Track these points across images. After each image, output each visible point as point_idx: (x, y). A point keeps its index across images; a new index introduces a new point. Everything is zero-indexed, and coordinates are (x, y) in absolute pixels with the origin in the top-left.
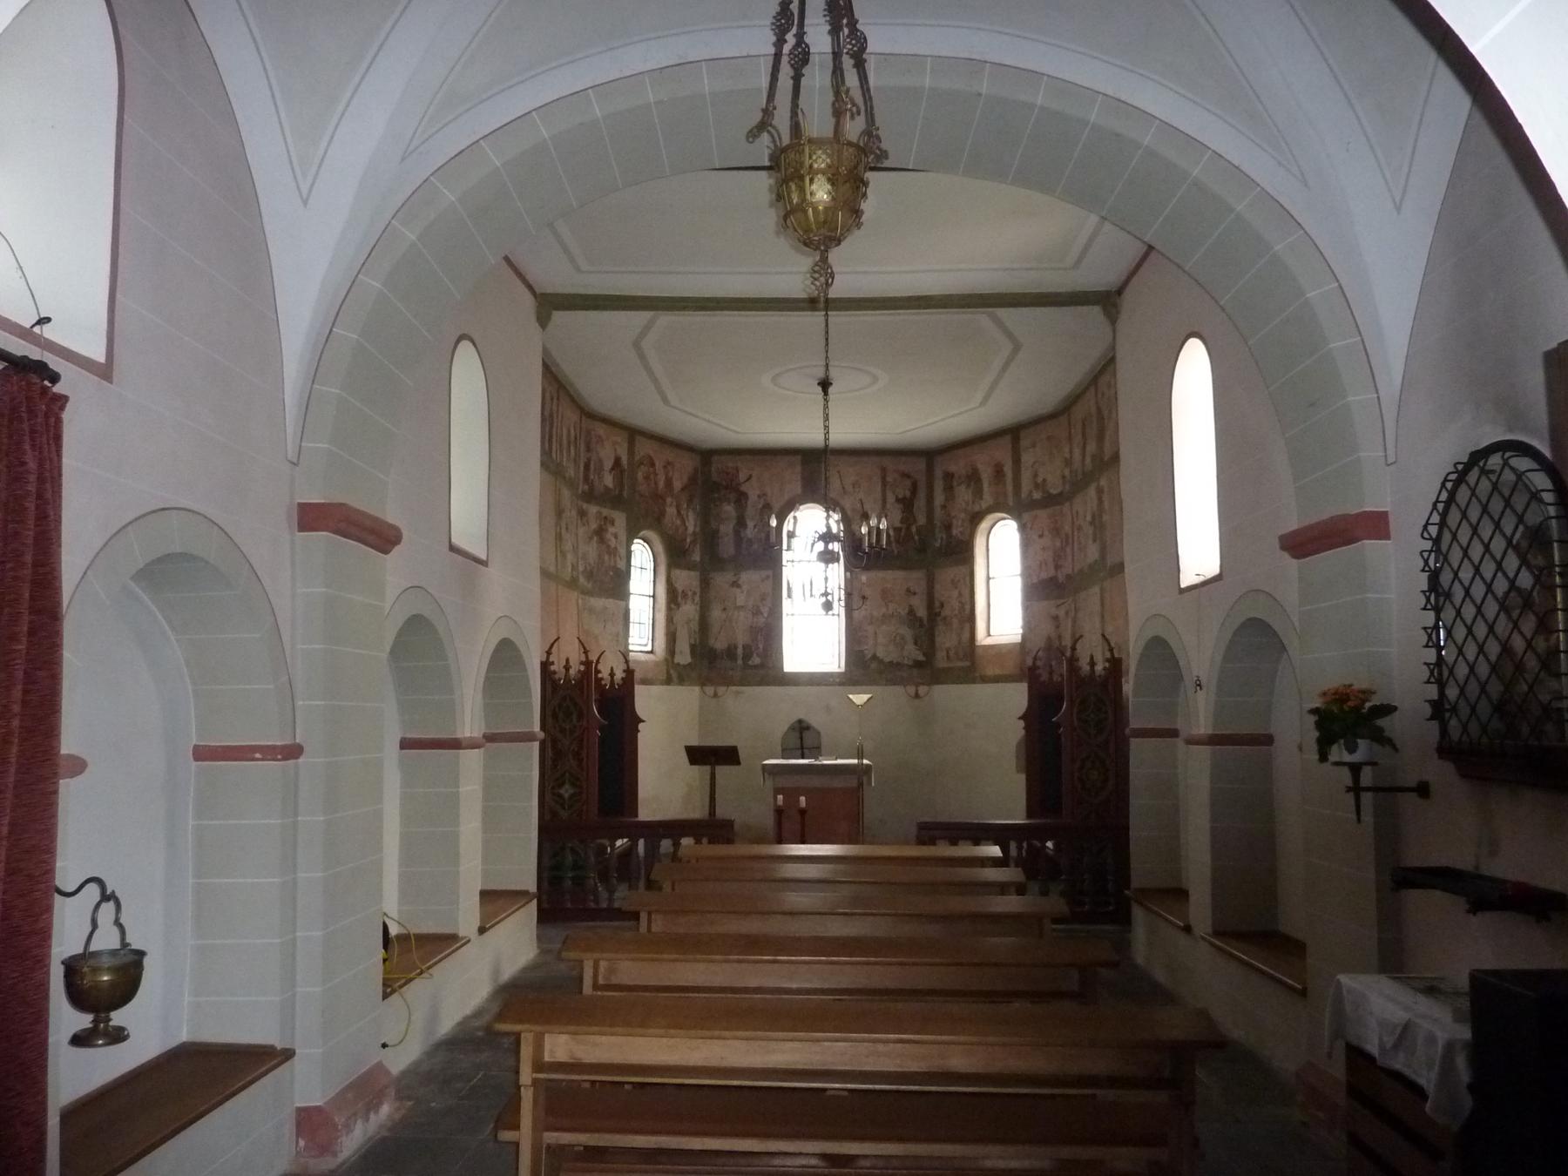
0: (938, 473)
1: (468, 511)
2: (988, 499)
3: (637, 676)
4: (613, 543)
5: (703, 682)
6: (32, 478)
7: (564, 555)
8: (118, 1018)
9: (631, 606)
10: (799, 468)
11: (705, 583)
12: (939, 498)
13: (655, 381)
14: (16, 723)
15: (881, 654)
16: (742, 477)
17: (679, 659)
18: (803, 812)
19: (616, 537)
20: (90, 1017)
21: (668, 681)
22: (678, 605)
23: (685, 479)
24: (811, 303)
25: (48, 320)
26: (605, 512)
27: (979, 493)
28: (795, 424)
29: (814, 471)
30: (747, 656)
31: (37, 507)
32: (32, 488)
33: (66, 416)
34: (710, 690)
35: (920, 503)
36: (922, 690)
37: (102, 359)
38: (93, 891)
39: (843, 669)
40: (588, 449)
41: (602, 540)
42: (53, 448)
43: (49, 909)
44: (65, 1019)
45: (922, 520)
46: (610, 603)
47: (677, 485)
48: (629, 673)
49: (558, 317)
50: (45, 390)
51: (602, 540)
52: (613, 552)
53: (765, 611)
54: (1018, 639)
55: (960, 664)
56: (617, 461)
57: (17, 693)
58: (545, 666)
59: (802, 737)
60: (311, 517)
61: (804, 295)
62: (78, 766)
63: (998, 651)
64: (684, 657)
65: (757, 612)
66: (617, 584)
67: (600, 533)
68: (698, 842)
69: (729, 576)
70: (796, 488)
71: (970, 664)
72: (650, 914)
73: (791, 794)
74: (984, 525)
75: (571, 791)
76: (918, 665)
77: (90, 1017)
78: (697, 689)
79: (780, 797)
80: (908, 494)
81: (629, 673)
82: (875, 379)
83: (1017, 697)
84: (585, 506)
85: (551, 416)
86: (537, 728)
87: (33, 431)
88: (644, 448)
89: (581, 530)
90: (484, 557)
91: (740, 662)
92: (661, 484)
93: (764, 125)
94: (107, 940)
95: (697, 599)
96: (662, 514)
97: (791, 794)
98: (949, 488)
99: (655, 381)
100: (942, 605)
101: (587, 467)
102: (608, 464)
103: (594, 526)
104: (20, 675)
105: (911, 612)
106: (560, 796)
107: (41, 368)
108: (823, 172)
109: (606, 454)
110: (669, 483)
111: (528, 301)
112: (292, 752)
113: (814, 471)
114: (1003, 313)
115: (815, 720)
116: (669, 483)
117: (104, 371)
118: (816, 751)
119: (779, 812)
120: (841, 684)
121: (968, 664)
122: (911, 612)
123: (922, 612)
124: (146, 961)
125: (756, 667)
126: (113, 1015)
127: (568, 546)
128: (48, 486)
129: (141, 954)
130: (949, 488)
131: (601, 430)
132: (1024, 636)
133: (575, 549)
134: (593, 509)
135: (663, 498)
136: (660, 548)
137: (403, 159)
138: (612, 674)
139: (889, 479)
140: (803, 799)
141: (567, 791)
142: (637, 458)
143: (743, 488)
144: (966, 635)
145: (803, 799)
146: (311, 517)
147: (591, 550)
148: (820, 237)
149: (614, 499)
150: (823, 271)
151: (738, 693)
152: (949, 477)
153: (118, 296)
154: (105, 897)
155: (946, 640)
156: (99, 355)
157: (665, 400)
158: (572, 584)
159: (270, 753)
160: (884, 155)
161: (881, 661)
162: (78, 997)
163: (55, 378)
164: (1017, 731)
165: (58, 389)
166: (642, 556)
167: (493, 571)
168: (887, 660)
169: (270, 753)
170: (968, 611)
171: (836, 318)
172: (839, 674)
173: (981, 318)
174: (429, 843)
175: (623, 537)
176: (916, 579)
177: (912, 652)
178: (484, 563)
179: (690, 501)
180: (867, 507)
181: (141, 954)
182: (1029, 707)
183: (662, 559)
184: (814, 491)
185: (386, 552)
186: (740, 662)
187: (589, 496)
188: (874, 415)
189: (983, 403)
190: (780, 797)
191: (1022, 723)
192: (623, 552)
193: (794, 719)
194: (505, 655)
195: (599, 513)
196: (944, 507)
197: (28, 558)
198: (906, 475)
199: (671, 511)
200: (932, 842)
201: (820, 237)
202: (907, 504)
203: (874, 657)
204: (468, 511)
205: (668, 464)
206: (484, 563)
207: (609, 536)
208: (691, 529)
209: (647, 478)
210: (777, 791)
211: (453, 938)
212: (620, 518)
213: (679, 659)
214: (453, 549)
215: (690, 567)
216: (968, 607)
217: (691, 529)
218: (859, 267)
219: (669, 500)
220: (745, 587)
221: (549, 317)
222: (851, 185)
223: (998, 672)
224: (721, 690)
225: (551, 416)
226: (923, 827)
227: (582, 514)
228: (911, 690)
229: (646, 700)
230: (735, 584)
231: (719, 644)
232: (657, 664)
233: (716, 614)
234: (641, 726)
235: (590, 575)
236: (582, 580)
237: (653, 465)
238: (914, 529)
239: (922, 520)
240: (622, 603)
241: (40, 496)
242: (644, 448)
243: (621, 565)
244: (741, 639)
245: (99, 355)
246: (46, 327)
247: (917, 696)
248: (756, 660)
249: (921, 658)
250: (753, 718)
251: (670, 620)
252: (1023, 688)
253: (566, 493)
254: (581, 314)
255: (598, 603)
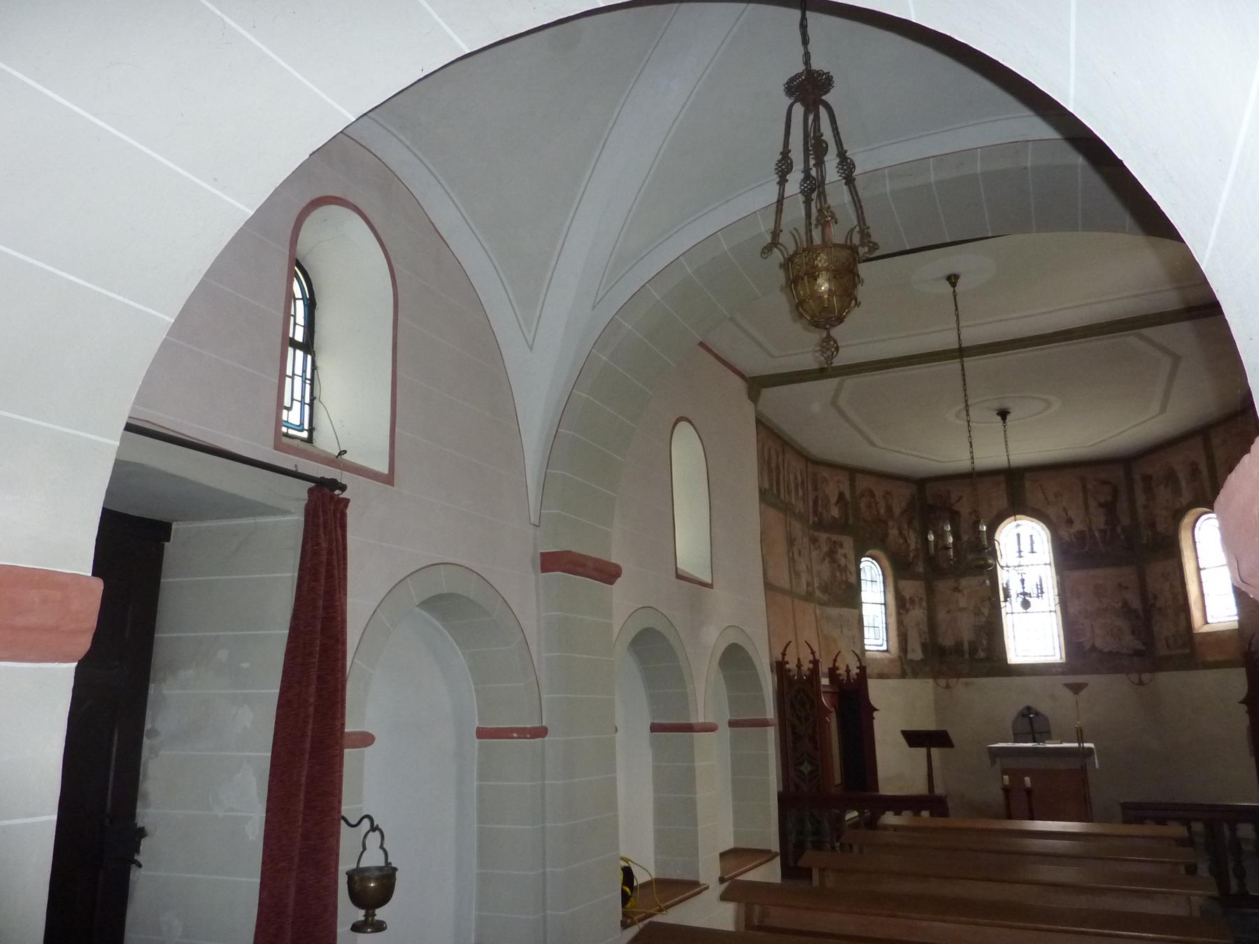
0: (1137, 477)
1: (691, 545)
2: (1186, 497)
3: (868, 671)
4: (843, 562)
5: (936, 676)
6: (325, 553)
7: (798, 574)
8: (381, 914)
9: (864, 612)
10: (1003, 486)
11: (930, 591)
12: (1141, 498)
13: (859, 431)
14: (311, 709)
15: (1099, 644)
16: (954, 497)
17: (910, 656)
18: (1029, 792)
19: (845, 556)
20: (362, 912)
21: (903, 675)
22: (908, 611)
23: (904, 504)
24: (821, 373)
25: (345, 452)
26: (835, 537)
27: (1177, 492)
28: (992, 452)
29: (1017, 489)
30: (973, 650)
31: (327, 571)
32: (324, 558)
33: (349, 511)
34: (942, 682)
35: (1123, 505)
36: (1146, 677)
37: (386, 472)
38: (366, 824)
39: (1064, 660)
40: (815, 489)
41: (833, 561)
42: (339, 532)
43: (336, 834)
44: (348, 912)
45: (1126, 521)
46: (846, 611)
47: (897, 511)
48: (862, 669)
49: (767, 393)
50: (332, 497)
51: (833, 561)
52: (844, 569)
53: (986, 611)
54: (1235, 625)
55: (1179, 651)
56: (841, 496)
57: (312, 689)
58: (779, 667)
59: (1031, 722)
60: (550, 562)
61: (816, 366)
62: (366, 740)
63: (1218, 638)
64: (916, 654)
65: (978, 613)
66: (850, 595)
67: (831, 554)
68: (931, 815)
69: (950, 583)
70: (1003, 502)
71: (1192, 650)
72: (822, 870)
73: (1016, 775)
74: (1187, 520)
75: (806, 772)
76: (1138, 653)
77: (362, 912)
78: (931, 681)
79: (1006, 777)
80: (1109, 498)
81: (862, 669)
82: (1049, 404)
83: (1237, 682)
84: (816, 534)
85: (778, 467)
86: (771, 713)
87: (325, 523)
88: (863, 483)
89: (814, 554)
90: (709, 581)
91: (967, 656)
92: (882, 511)
93: (775, 243)
94: (373, 859)
95: (924, 604)
96: (886, 535)
97: (1016, 775)
98: (1148, 490)
99: (859, 431)
100: (1156, 597)
101: (815, 502)
102: (834, 499)
103: (825, 549)
104: (314, 677)
105: (1125, 604)
106: (801, 772)
107: (334, 484)
108: (827, 270)
109: (832, 492)
110: (889, 509)
111: (739, 385)
112: (540, 732)
113: (1017, 489)
114: (1147, 332)
115: (1043, 707)
116: (889, 509)
117: (389, 479)
118: (1047, 735)
119: (1006, 790)
120: (1063, 674)
121: (1187, 651)
122: (1125, 604)
123: (1136, 604)
124: (398, 874)
125: (982, 660)
126: (377, 911)
127: (802, 567)
128: (335, 557)
129: (395, 869)
130: (1148, 490)
131: (825, 473)
132: (1240, 622)
133: (809, 570)
134: (823, 536)
135: (886, 523)
136: (886, 563)
137: (594, 307)
138: (848, 671)
139: (1089, 486)
140: (1027, 779)
141: (806, 768)
142: (858, 492)
143: (955, 508)
144: (1183, 625)
145: (1027, 779)
146: (550, 562)
147: (825, 569)
148: (824, 318)
149: (841, 527)
150: (830, 347)
151: (967, 684)
152: (1147, 479)
153: (397, 430)
154: (374, 828)
155: (1164, 629)
156: (383, 468)
157: (872, 444)
158: (809, 597)
159: (523, 733)
160: (874, 247)
161: (1101, 652)
162: (358, 898)
163: (343, 488)
164: (1240, 719)
165: (345, 495)
166: (871, 573)
167: (716, 591)
168: (1106, 650)
169: (523, 733)
170: (1181, 602)
171: (970, 362)
172: (1060, 665)
173: (1130, 339)
174: (675, 810)
175: (852, 556)
176: (1127, 574)
177: (1130, 642)
178: (710, 586)
179: (910, 523)
180: (1071, 514)
181: (395, 869)
182: (1250, 690)
183: (889, 572)
184: (1018, 506)
185: (612, 583)
186: (967, 656)
187: (820, 525)
188: (1047, 435)
189: (1163, 409)
190: (1006, 777)
191: (1244, 708)
192: (853, 569)
193: (1021, 707)
194: (734, 659)
195: (829, 539)
196: (1145, 507)
197: (320, 603)
198: (1105, 482)
199: (893, 532)
200: (1140, 821)
201: (824, 318)
202: (1109, 508)
203: (1093, 648)
204: (691, 545)
205: (887, 494)
206: (710, 586)
207: (839, 556)
208: (913, 546)
209: (869, 506)
210: (1004, 772)
211: (695, 884)
212: (848, 543)
213: (910, 656)
214: (680, 576)
215: (915, 577)
216: (1180, 598)
217: (913, 546)
218: (857, 340)
219: (891, 524)
220: (965, 592)
221: (759, 393)
222: (847, 277)
223: (1220, 657)
224: (953, 681)
225: (778, 467)
226: (1125, 806)
227: (814, 540)
228: (1134, 677)
229: (877, 691)
230: (957, 589)
231: (947, 641)
232: (891, 661)
233: (942, 615)
234: (875, 714)
235: (825, 589)
236: (818, 594)
237: (873, 495)
238: (1119, 530)
239: (1126, 521)
240: (856, 611)
241: (329, 563)
242: (863, 483)
243: (853, 580)
244: (967, 635)
245: (383, 468)
246: (345, 456)
247: (1141, 683)
248: (982, 655)
249: (1140, 647)
250: (983, 707)
251: (900, 623)
252: (1242, 672)
253: (797, 526)
254: (795, 387)
255: (834, 612)
